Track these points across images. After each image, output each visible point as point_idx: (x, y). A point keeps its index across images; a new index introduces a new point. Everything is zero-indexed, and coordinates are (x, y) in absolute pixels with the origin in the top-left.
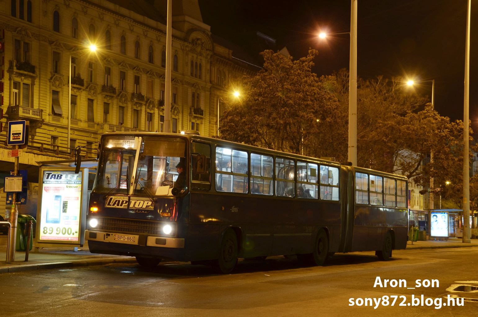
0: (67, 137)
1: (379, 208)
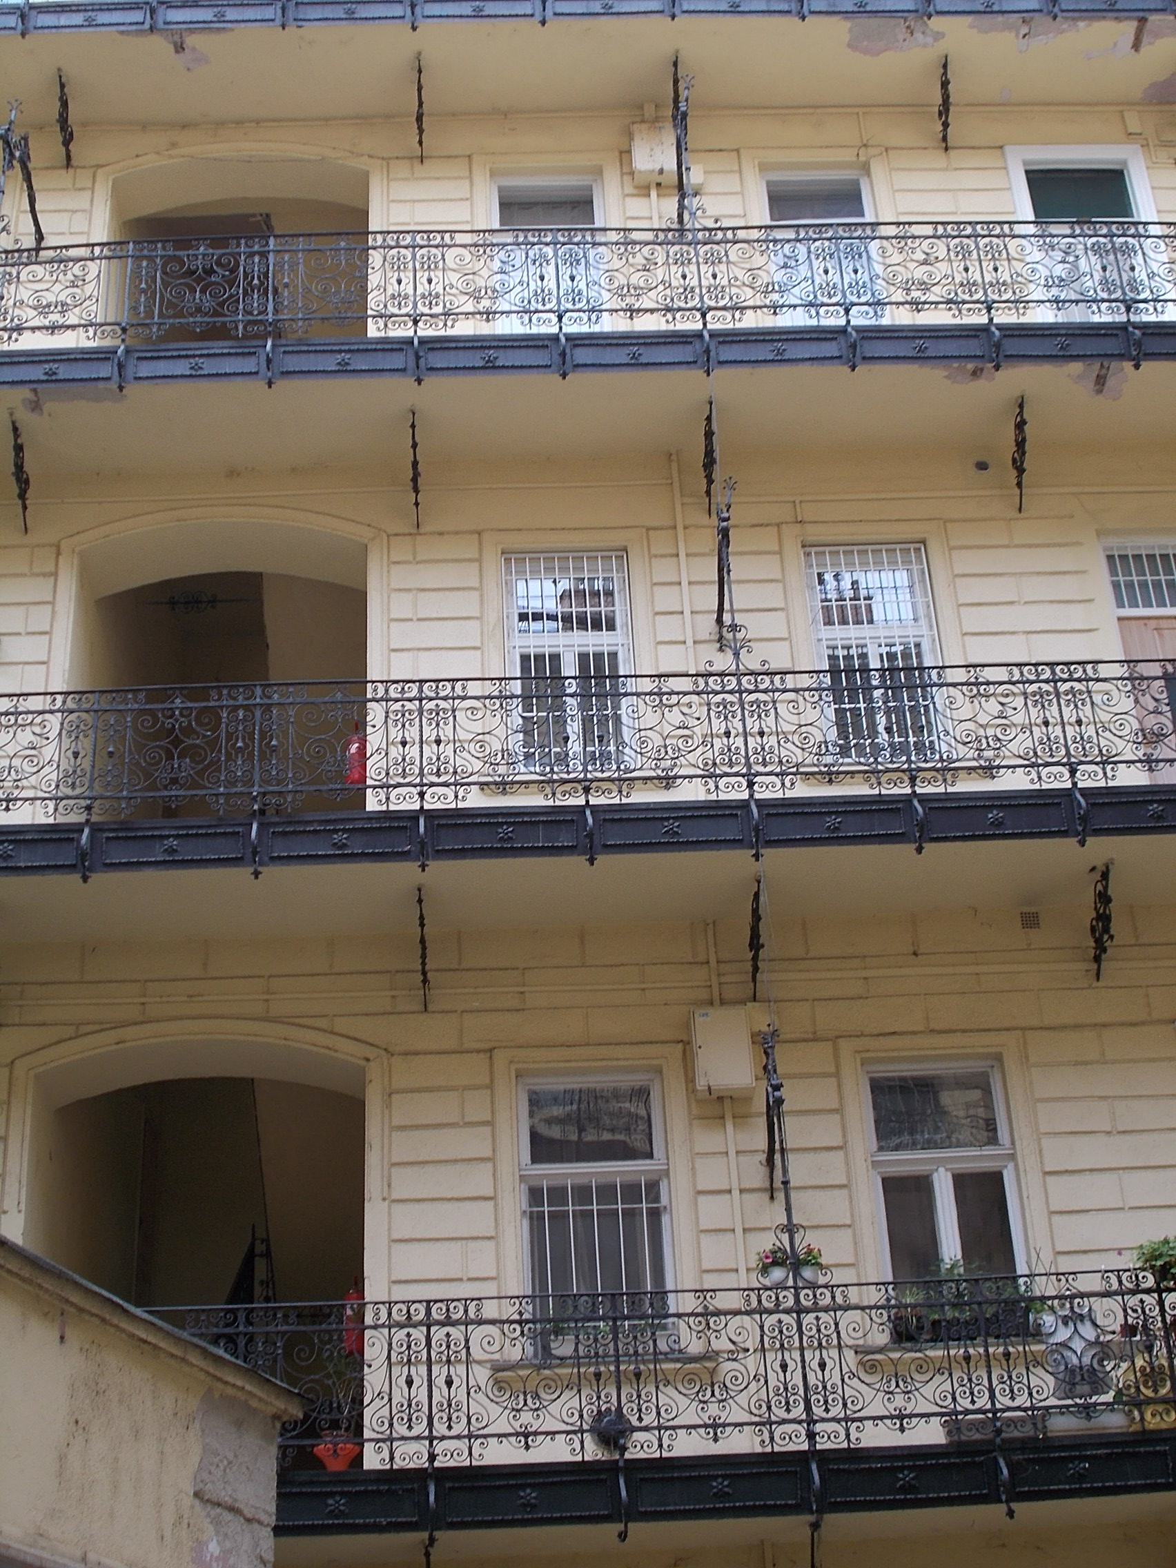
0: (488, 1159)
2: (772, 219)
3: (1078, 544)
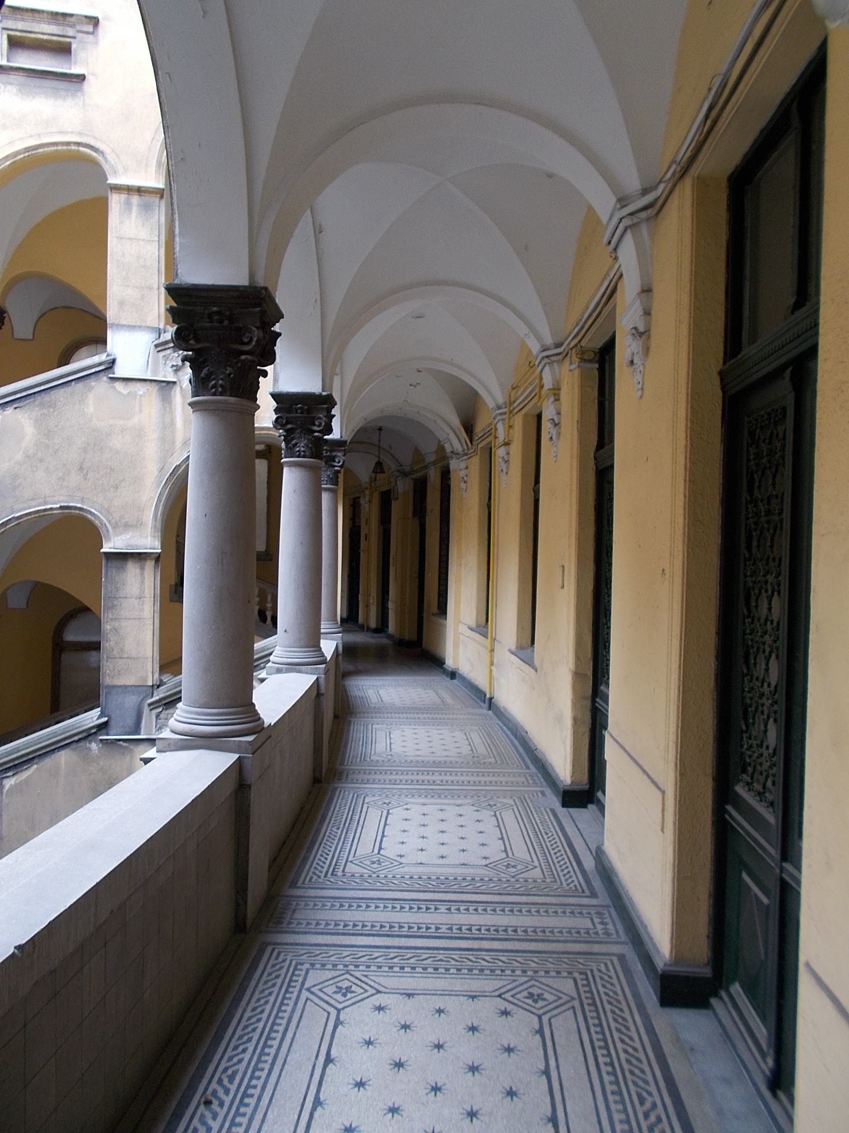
1: (309, 212)
2: (70, 43)
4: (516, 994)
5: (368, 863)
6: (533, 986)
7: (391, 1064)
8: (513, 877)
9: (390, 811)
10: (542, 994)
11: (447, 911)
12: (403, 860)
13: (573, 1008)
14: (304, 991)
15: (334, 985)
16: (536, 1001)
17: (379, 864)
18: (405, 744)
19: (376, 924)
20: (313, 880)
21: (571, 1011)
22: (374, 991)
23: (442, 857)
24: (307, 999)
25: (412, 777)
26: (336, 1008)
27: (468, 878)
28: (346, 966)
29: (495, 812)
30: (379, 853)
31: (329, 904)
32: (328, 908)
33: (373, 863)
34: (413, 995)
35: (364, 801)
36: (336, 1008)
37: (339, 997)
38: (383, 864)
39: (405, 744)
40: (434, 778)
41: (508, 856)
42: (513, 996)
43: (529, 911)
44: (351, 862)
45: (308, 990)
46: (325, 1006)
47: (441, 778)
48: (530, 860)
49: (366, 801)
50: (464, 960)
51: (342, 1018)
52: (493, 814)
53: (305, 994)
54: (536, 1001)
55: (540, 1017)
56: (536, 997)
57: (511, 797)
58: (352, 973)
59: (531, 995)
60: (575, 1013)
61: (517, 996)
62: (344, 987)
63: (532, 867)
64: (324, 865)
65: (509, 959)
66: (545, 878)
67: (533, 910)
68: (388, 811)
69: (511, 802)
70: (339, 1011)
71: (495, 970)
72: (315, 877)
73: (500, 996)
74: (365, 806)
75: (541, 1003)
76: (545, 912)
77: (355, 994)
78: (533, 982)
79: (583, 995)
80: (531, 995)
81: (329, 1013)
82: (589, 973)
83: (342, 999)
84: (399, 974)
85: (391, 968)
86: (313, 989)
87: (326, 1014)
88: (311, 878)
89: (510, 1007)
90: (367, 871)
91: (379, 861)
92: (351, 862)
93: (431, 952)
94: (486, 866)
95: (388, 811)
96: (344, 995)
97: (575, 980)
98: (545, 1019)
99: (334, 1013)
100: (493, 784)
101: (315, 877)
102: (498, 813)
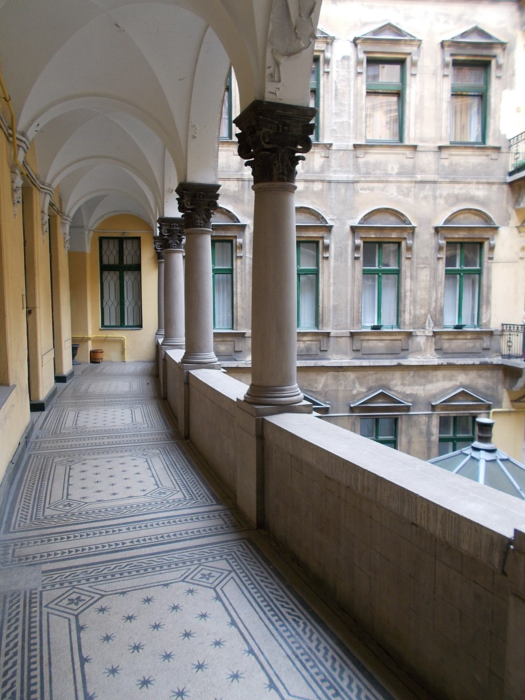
0: (401, 139)
3: (140, 330)
4: (193, 577)
5: (61, 506)
6: (202, 569)
7: (229, 625)
8: (165, 500)
9: (72, 467)
10: (79, 597)
11: (127, 531)
12: (85, 500)
13: (232, 578)
14: (43, 608)
15: (66, 599)
16: (208, 579)
17: (70, 506)
18: (123, 414)
19: (51, 553)
20: (22, 525)
21: (232, 580)
22: (50, 606)
23: (114, 494)
24: (48, 613)
25: (123, 439)
26: (73, 615)
27: (134, 506)
28: (71, 583)
29: (146, 459)
30: (67, 499)
31: (26, 542)
32: (32, 544)
33: (65, 506)
34: (168, 584)
35: (53, 460)
36: (73, 615)
37: (73, 606)
38: (72, 506)
39: (123, 414)
40: (108, 440)
41: (159, 487)
42: (192, 579)
43: (192, 519)
44: (48, 508)
45: (46, 606)
46: (64, 615)
47: (104, 441)
48: (174, 487)
49: (54, 461)
50: (172, 559)
51: (81, 623)
52: (145, 460)
53: (45, 610)
54: (208, 579)
55: (214, 589)
56: (207, 576)
57: (157, 449)
58: (77, 587)
59: (72, 601)
60: (234, 580)
61: (194, 578)
62: (75, 598)
63: (176, 492)
64: (21, 516)
65: (210, 550)
66: (185, 497)
67: (182, 520)
68: (70, 466)
69: (158, 451)
70: (77, 616)
71: (80, 580)
72: (22, 523)
73: (183, 581)
74: (54, 464)
75: (211, 580)
76: (196, 519)
77: (85, 602)
78: (201, 567)
79: (235, 568)
80: (72, 601)
81: (69, 620)
82: (233, 553)
83: (75, 607)
84: (152, 573)
85: (113, 576)
86: (50, 606)
87: (67, 620)
88: (19, 524)
89: (192, 587)
90: (62, 512)
91: (69, 504)
92: (48, 508)
93: (106, 564)
94: (145, 495)
95: (70, 466)
96: (77, 604)
97: (226, 559)
98: (218, 589)
99: (72, 618)
100: (151, 440)
101: (22, 524)
102: (149, 460)
